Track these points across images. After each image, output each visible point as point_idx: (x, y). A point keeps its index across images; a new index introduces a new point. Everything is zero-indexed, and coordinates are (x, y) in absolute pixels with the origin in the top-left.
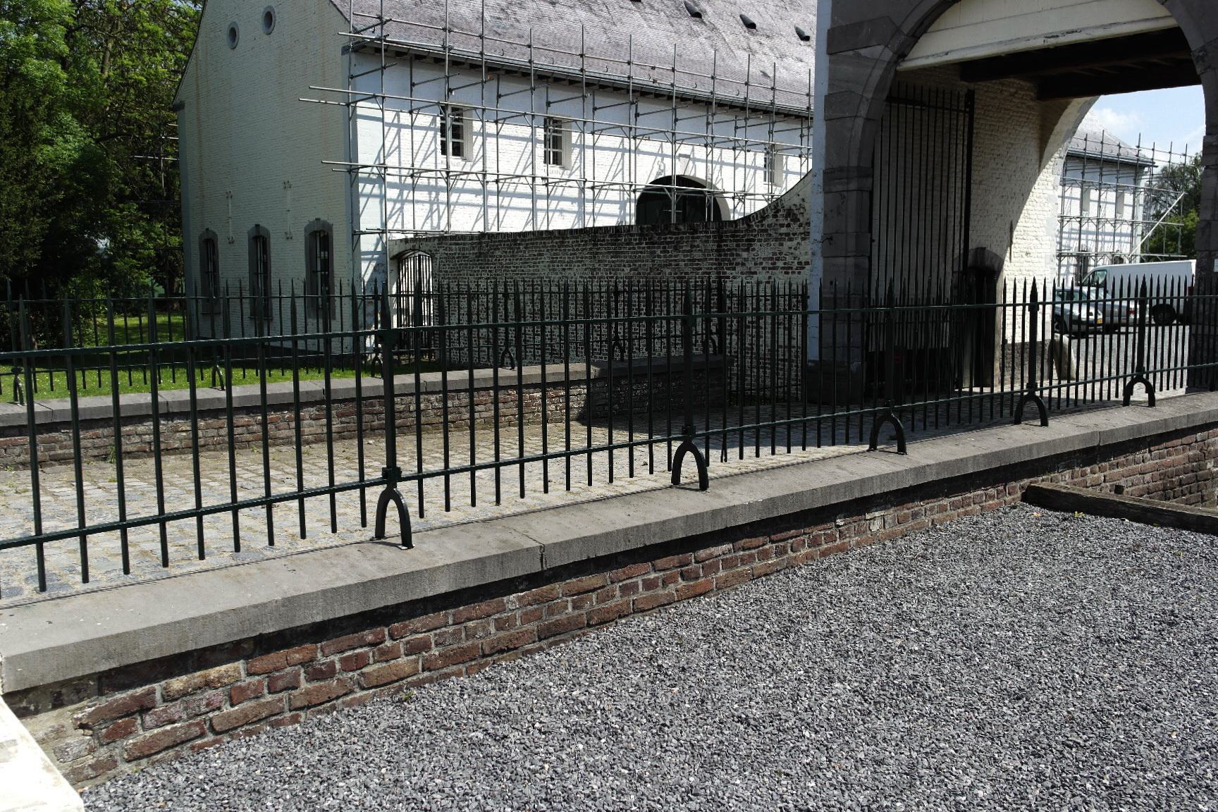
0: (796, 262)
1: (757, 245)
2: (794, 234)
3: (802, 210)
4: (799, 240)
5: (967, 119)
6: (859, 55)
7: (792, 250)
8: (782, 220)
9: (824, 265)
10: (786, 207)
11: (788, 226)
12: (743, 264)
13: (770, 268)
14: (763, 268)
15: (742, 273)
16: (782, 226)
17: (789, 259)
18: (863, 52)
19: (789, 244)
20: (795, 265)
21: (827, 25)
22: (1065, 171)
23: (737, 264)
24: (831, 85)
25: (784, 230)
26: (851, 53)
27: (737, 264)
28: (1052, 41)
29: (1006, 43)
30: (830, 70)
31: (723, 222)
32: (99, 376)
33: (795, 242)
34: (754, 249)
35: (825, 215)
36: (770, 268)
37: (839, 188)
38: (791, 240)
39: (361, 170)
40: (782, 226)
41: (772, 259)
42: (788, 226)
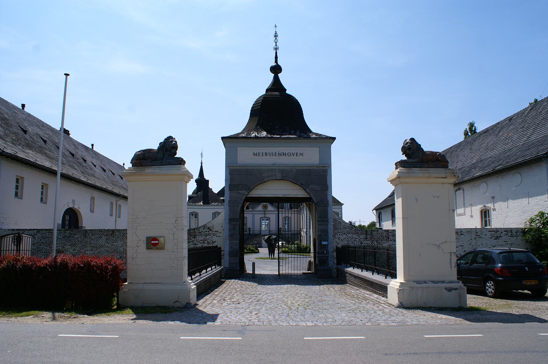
0: (211, 241)
1: (198, 237)
2: (210, 234)
3: (213, 228)
4: (212, 236)
5: (268, 212)
6: (239, 192)
7: (210, 238)
8: (206, 230)
9: (229, 242)
10: (208, 227)
11: (209, 232)
12: (192, 242)
13: (202, 243)
14: (200, 243)
15: (192, 244)
16: (206, 232)
17: (209, 241)
18: (240, 191)
19: (209, 236)
20: (211, 242)
21: (229, 183)
22: (237, 162)
23: (191, 242)
24: (230, 198)
25: (207, 233)
26: (236, 191)
27: (191, 242)
28: (285, 196)
29: (275, 195)
30: (230, 194)
31: (86, 231)
32: (471, 208)
33: (211, 236)
34: (196, 238)
35: (229, 230)
36: (202, 243)
37: (234, 223)
38: (210, 235)
39: (280, 226)
40: (206, 232)
41: (203, 240)
42: (209, 232)
